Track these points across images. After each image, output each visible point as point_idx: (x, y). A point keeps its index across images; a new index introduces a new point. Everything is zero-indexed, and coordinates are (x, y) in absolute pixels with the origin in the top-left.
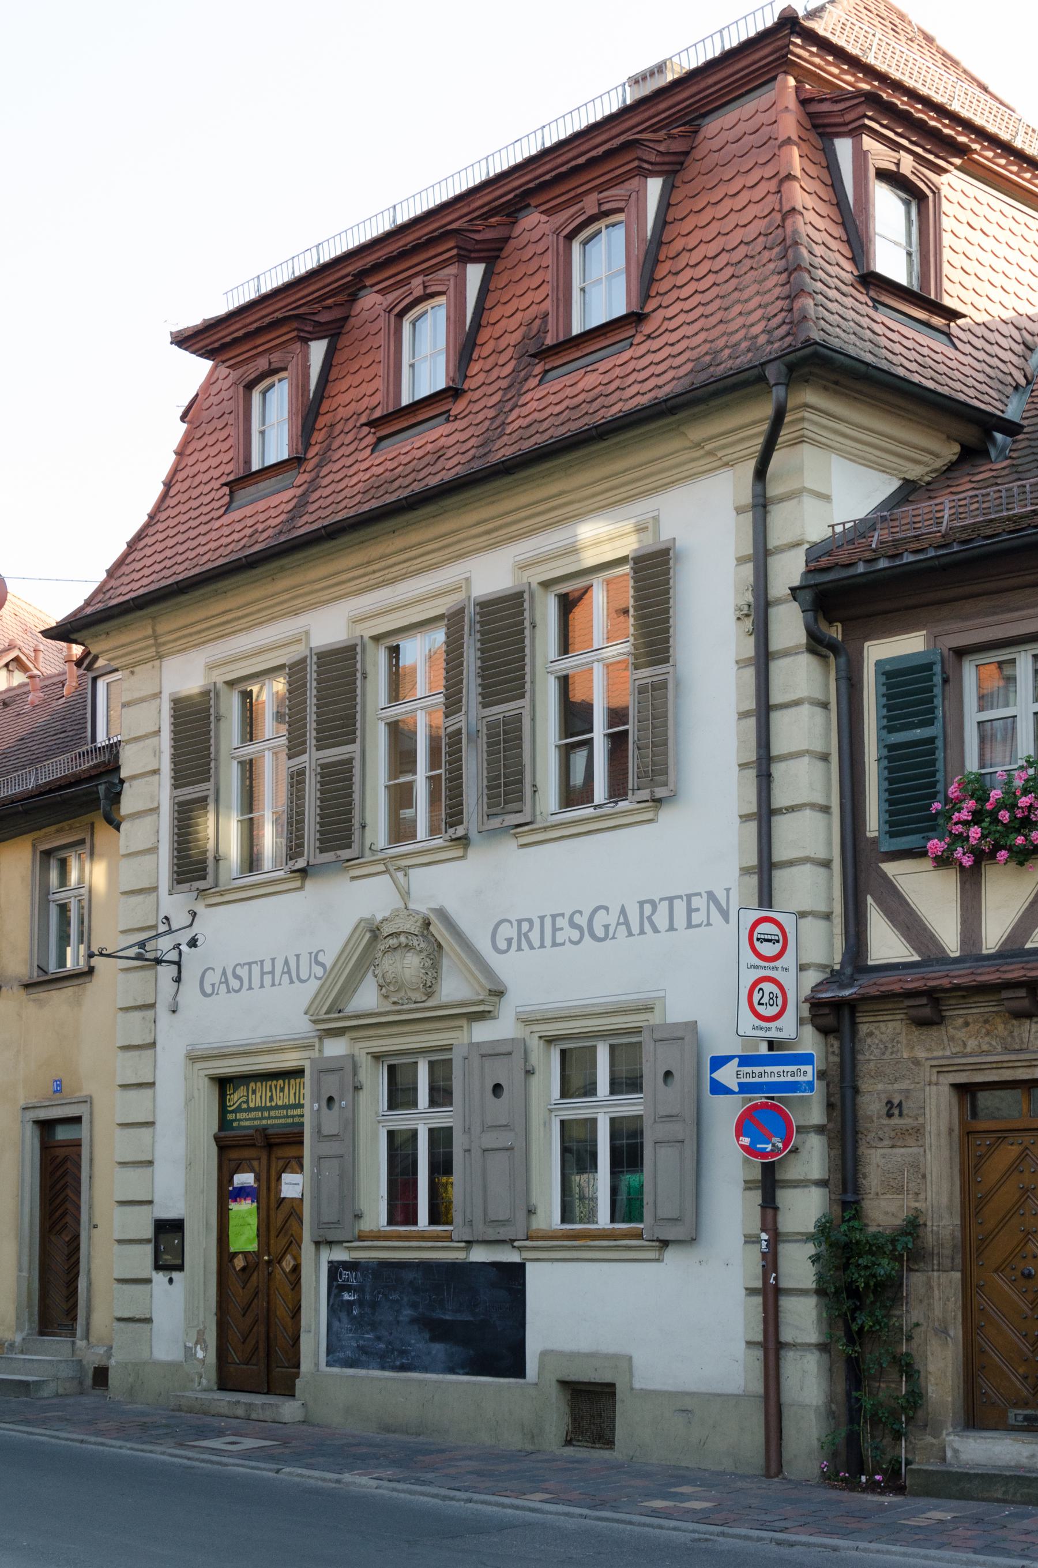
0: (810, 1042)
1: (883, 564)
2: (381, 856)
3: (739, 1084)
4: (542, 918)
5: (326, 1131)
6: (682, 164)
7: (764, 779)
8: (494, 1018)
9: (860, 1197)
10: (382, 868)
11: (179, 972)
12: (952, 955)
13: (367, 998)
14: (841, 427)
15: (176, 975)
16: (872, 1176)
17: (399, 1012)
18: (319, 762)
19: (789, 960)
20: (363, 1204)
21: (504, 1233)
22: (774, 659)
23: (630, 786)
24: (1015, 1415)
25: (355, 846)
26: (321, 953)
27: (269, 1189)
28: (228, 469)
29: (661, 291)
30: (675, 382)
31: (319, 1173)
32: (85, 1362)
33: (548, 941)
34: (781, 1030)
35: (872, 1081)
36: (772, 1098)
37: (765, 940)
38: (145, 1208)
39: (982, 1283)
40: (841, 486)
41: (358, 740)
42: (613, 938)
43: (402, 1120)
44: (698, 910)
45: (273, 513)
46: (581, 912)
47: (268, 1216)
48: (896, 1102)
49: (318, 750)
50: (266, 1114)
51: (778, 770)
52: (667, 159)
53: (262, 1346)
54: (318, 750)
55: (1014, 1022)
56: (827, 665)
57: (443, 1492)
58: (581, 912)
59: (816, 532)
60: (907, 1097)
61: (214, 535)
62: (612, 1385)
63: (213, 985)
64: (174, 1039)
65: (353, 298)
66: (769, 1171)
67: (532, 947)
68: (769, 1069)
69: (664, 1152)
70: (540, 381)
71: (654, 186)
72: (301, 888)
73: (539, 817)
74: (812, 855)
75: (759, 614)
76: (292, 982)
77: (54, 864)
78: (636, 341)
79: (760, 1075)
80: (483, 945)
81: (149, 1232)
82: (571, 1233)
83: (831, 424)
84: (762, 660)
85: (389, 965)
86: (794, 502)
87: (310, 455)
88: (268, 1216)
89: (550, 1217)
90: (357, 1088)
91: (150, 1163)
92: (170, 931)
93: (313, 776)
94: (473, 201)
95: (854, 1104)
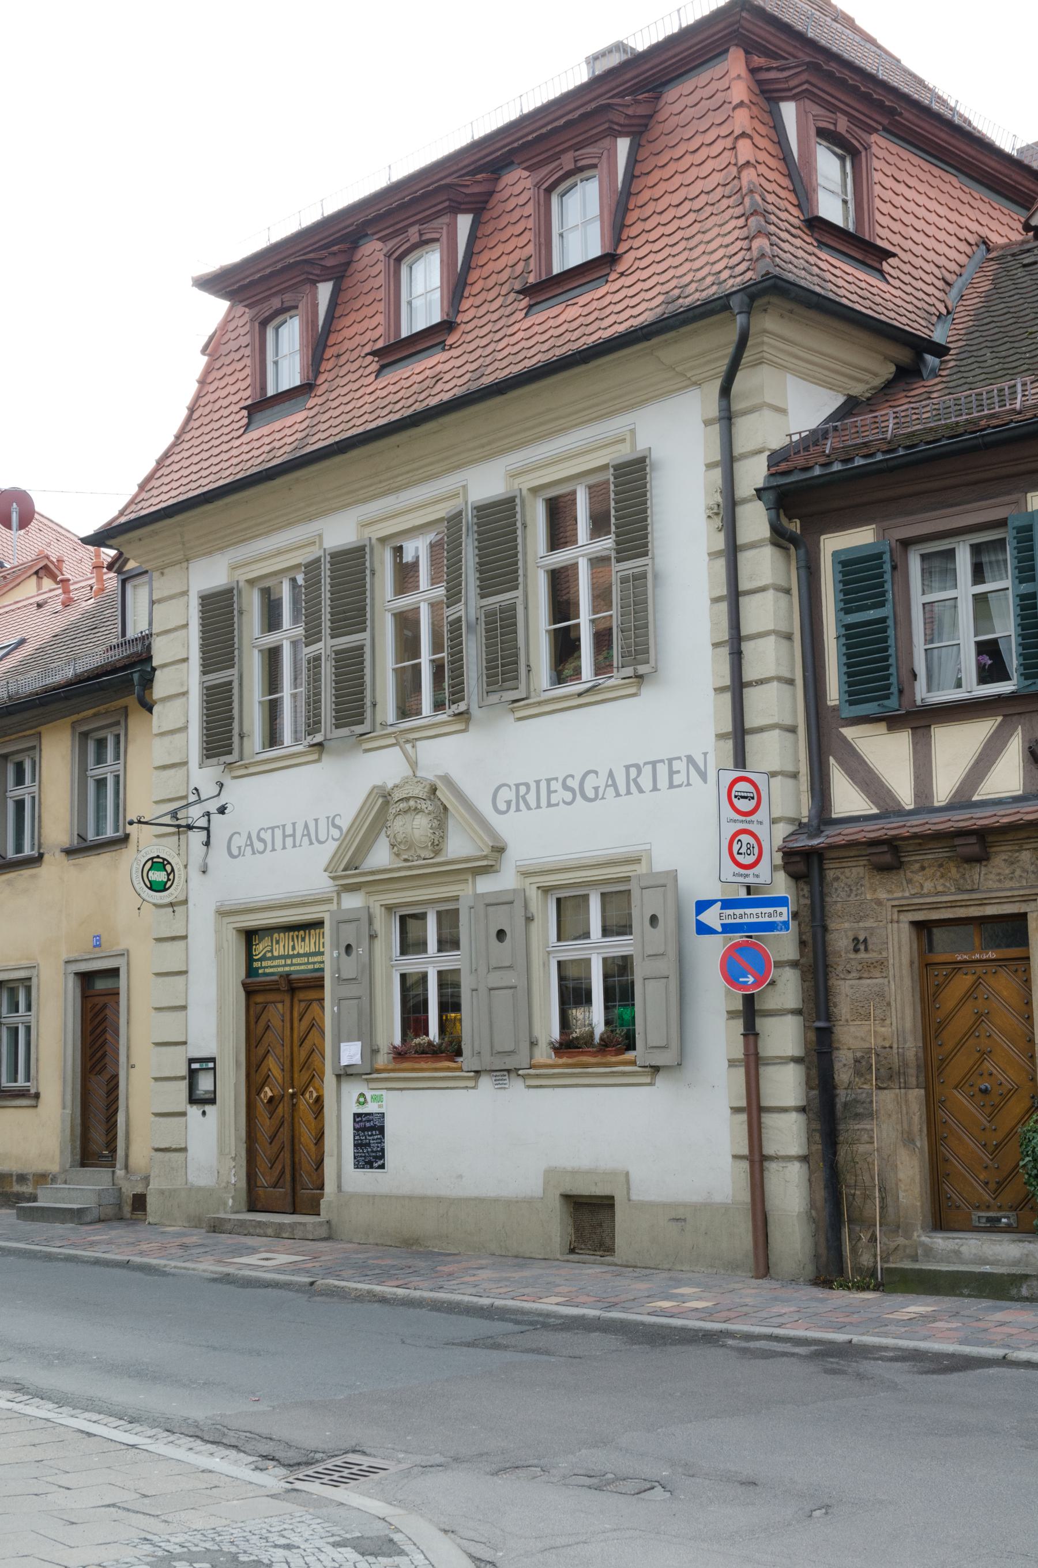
0: (781, 886)
1: (837, 467)
3: (722, 925)
4: (538, 782)
6: (646, 125)
8: (497, 871)
10: (393, 741)
12: (907, 808)
13: (380, 856)
14: (795, 350)
17: (410, 868)
18: (334, 649)
19: (762, 814)
21: (510, 1063)
23: (615, 665)
27: (292, 1029)
34: (758, 876)
36: (750, 937)
37: (742, 795)
39: (943, 1099)
40: (794, 403)
41: (368, 629)
42: (603, 798)
44: (678, 772)
46: (572, 776)
50: (289, 962)
54: (332, 638)
55: (966, 865)
56: (788, 557)
58: (572, 776)
59: (777, 442)
60: (872, 934)
63: (239, 848)
65: (355, 246)
66: (749, 1000)
67: (529, 808)
68: (748, 911)
69: (651, 985)
70: (526, 314)
73: (533, 694)
76: (311, 843)
78: (611, 278)
79: (741, 917)
80: (485, 808)
81: (183, 1071)
85: (399, 826)
86: (757, 414)
87: (319, 382)
90: (373, 937)
91: (184, 1008)
92: (199, 801)
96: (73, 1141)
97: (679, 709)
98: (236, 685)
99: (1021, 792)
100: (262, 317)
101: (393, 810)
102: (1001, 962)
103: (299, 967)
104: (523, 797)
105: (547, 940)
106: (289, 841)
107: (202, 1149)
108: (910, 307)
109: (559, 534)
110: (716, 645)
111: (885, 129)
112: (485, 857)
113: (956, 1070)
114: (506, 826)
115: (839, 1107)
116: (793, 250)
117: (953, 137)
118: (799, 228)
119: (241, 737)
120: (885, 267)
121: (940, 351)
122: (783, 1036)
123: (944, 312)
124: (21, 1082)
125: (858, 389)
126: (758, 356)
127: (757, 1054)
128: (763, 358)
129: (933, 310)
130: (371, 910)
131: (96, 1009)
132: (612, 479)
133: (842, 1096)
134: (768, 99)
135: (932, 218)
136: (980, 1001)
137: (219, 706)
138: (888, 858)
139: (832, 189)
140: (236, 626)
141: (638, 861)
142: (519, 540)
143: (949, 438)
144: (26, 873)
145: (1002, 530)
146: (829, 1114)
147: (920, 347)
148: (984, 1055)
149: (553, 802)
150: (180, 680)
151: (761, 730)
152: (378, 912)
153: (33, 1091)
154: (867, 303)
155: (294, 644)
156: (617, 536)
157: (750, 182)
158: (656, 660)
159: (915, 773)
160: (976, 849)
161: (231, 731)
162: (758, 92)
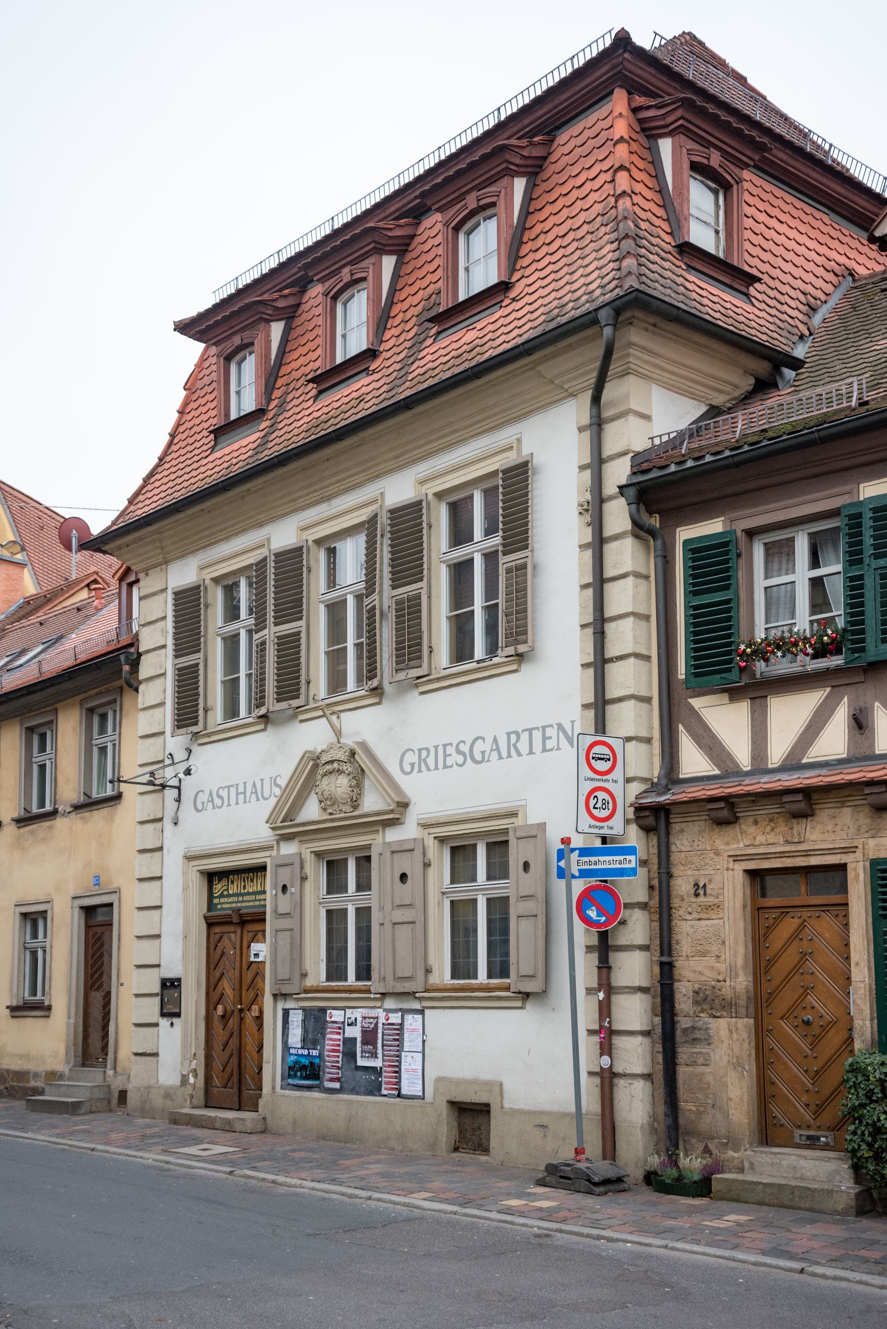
0: (634, 837)
1: (690, 464)
2: (321, 703)
3: (580, 870)
4: (436, 747)
5: (281, 910)
6: (541, 167)
7: (599, 635)
8: (402, 823)
9: (674, 959)
10: (320, 713)
11: (180, 794)
12: (745, 769)
13: (311, 811)
14: (659, 362)
15: (177, 796)
16: (684, 943)
17: (332, 820)
18: (277, 635)
19: (617, 774)
20: (308, 966)
21: (408, 987)
22: (607, 542)
23: (500, 645)
24: (799, 1134)
25: (302, 697)
26: (278, 778)
27: (241, 954)
28: (214, 421)
29: (524, 265)
30: (531, 331)
31: (276, 942)
32: (112, 1087)
33: (441, 765)
34: (611, 828)
35: (682, 868)
36: (606, 881)
37: (598, 757)
38: (155, 970)
39: (771, 1028)
40: (658, 412)
41: (304, 618)
42: (488, 761)
43: (336, 901)
44: (550, 738)
45: (243, 450)
46: (464, 742)
47: (241, 976)
48: (701, 884)
49: (275, 625)
50: (240, 899)
51: (610, 628)
52: (530, 162)
53: (235, 1073)
54: (275, 625)
55: (794, 820)
56: (648, 548)
57: (350, 1191)
58: (464, 742)
59: (640, 444)
60: (710, 881)
61: (202, 469)
62: (488, 1105)
63: (203, 803)
64: (176, 844)
65: (303, 291)
66: (604, 936)
67: (429, 769)
68: (602, 858)
69: (524, 923)
70: (434, 340)
71: (519, 185)
72: (264, 730)
73: (434, 671)
74: (636, 693)
75: (595, 508)
76: (258, 800)
77: (96, 720)
78: (504, 304)
79: (595, 863)
80: (393, 769)
81: (157, 989)
82: (458, 986)
83: (652, 359)
84: (597, 544)
85: (327, 785)
86: (623, 420)
87: (270, 408)
88: (241, 976)
89: (443, 974)
90: (304, 879)
92: (173, 764)
93: (272, 646)
94: (388, 208)
95: (669, 886)
96: (75, 1044)
97: (552, 683)
98: (201, 667)
99: (845, 756)
100: (226, 353)
101: (321, 771)
102: (825, 907)
103: (247, 904)
104: (425, 760)
105: (442, 883)
106: (241, 797)
107: (165, 1054)
108: (772, 327)
109: (460, 534)
110: (583, 626)
111: (756, 167)
112: (392, 811)
113: (783, 1003)
114: (410, 785)
115: (678, 1032)
116: (660, 271)
117: (814, 170)
118: (670, 253)
119: (206, 711)
120: (752, 290)
121: (796, 364)
122: (633, 968)
123: (807, 333)
124: (39, 996)
125: (719, 400)
126: (625, 367)
127: (609, 984)
128: (629, 368)
129: (795, 331)
130: (303, 856)
131: (97, 936)
132: (501, 482)
133: (683, 1022)
134: (648, 137)
135: (802, 250)
136: (805, 941)
137: (188, 684)
138: (725, 814)
139: (704, 219)
140: (202, 617)
141: (514, 814)
142: (425, 538)
143: (788, 434)
144: (46, 824)
145: (838, 519)
146: (668, 1038)
147: (780, 360)
148: (806, 990)
149: (448, 764)
150: (159, 665)
151: (620, 700)
152: (309, 859)
153: (46, 1003)
154: (730, 321)
155: (250, 632)
156: (504, 532)
157: (626, 209)
158: (533, 641)
159: (752, 738)
160: (802, 806)
161: (197, 705)
162: (638, 130)
